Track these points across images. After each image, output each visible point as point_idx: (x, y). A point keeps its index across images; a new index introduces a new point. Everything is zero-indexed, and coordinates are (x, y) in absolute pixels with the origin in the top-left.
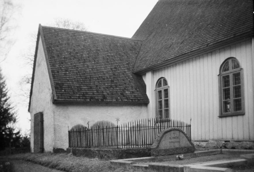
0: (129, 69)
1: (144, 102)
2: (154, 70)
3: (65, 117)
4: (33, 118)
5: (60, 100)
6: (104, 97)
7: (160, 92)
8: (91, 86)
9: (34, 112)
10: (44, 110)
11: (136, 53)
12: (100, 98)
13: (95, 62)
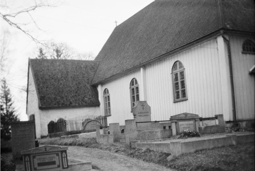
0: (88, 83)
1: (97, 104)
2: (102, 83)
3: (47, 117)
4: (168, 57)
5: (43, 106)
6: (71, 103)
7: (133, 89)
8: (63, 96)
9: (30, 115)
10: (35, 113)
11: (94, 71)
12: (68, 103)
13: (65, 80)
